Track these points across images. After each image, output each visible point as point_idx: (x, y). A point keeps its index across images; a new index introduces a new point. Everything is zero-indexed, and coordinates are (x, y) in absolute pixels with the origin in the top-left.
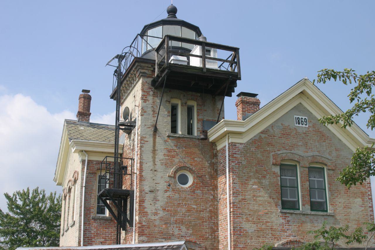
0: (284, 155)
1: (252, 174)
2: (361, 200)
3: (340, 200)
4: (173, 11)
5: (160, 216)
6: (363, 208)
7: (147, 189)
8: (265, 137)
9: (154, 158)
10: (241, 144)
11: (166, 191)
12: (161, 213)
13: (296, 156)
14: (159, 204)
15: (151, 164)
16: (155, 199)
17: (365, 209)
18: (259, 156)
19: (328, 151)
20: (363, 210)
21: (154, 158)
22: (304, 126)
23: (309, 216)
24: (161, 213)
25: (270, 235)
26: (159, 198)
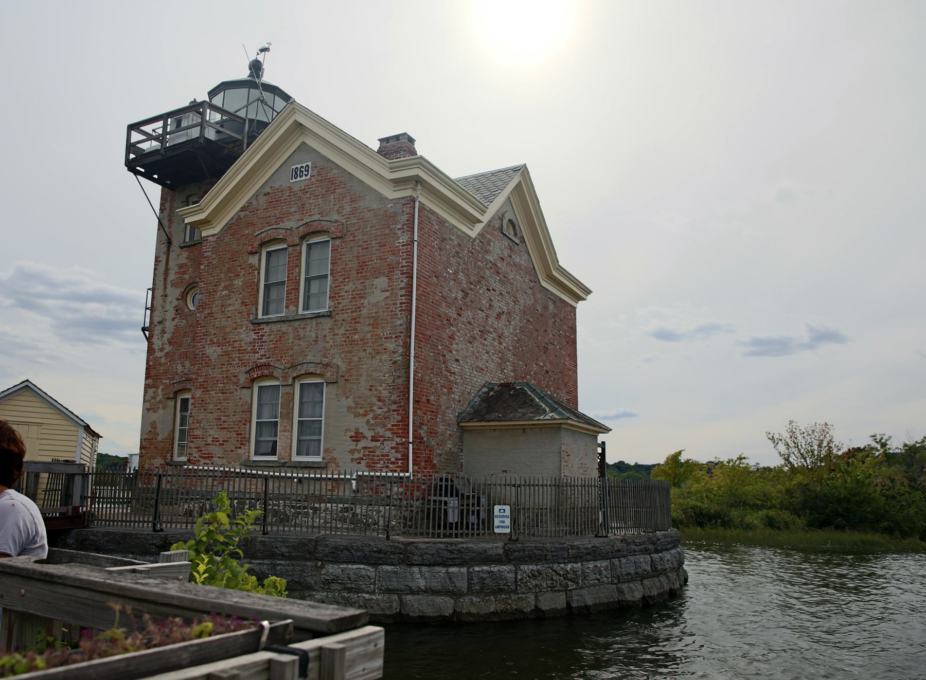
0: (263, 235)
1: (222, 276)
2: (386, 279)
3: (346, 288)
4: (256, 67)
5: (166, 351)
6: (388, 294)
7: (156, 320)
8: (246, 216)
9: (165, 279)
10: (213, 235)
11: (174, 319)
12: (168, 348)
13: (281, 231)
14: (167, 336)
15: (162, 288)
16: (163, 332)
17: (392, 294)
18: (234, 246)
19: (336, 208)
20: (386, 298)
21: (165, 279)
22: (304, 177)
23: (293, 323)
24: (168, 348)
25: (237, 359)
26: (167, 329)
